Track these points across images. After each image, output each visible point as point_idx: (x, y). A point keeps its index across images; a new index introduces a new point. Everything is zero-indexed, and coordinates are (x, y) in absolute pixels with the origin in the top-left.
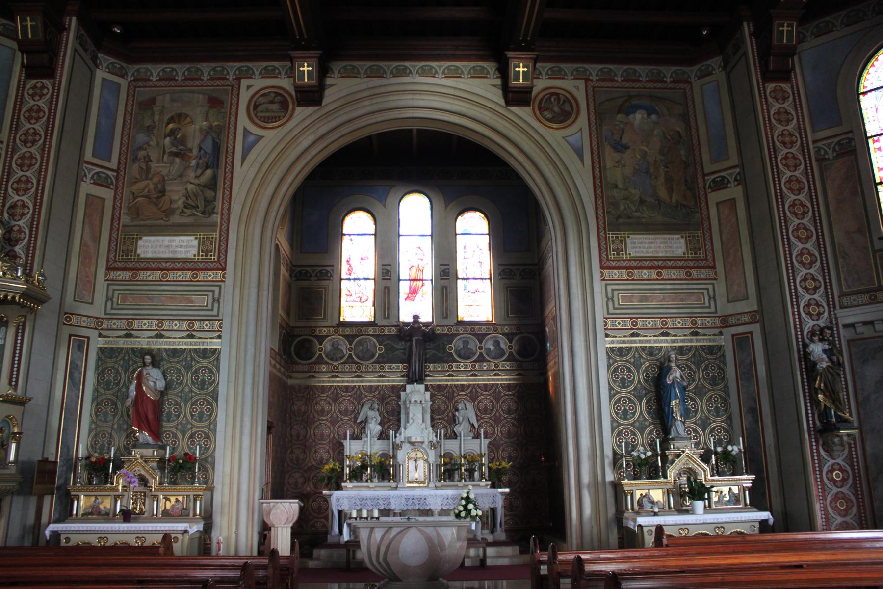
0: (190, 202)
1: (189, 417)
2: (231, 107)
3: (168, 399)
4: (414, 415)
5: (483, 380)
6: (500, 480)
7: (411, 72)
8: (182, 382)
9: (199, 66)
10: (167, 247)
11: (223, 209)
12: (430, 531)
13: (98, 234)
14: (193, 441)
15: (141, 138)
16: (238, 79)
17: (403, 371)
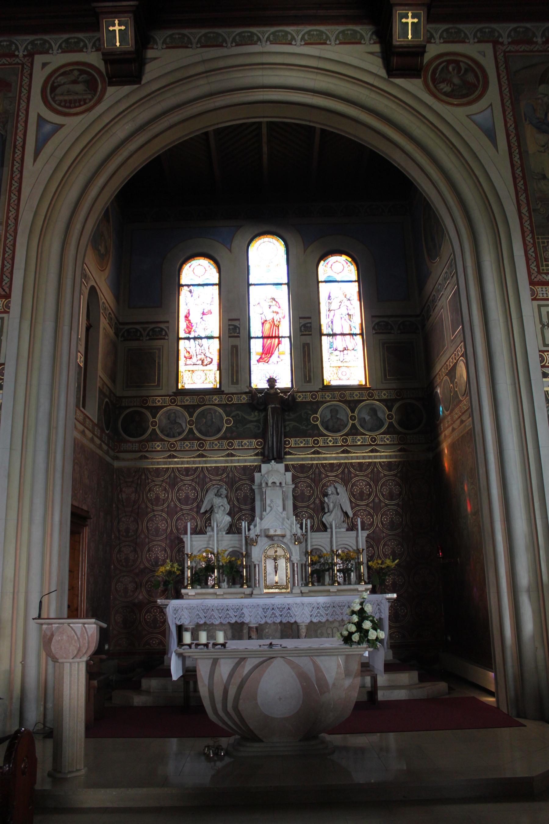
2: (20, 90)
4: (272, 501)
5: (357, 458)
6: (382, 582)
7: (259, 39)
12: (305, 663)
16: (31, 55)
17: (256, 448)
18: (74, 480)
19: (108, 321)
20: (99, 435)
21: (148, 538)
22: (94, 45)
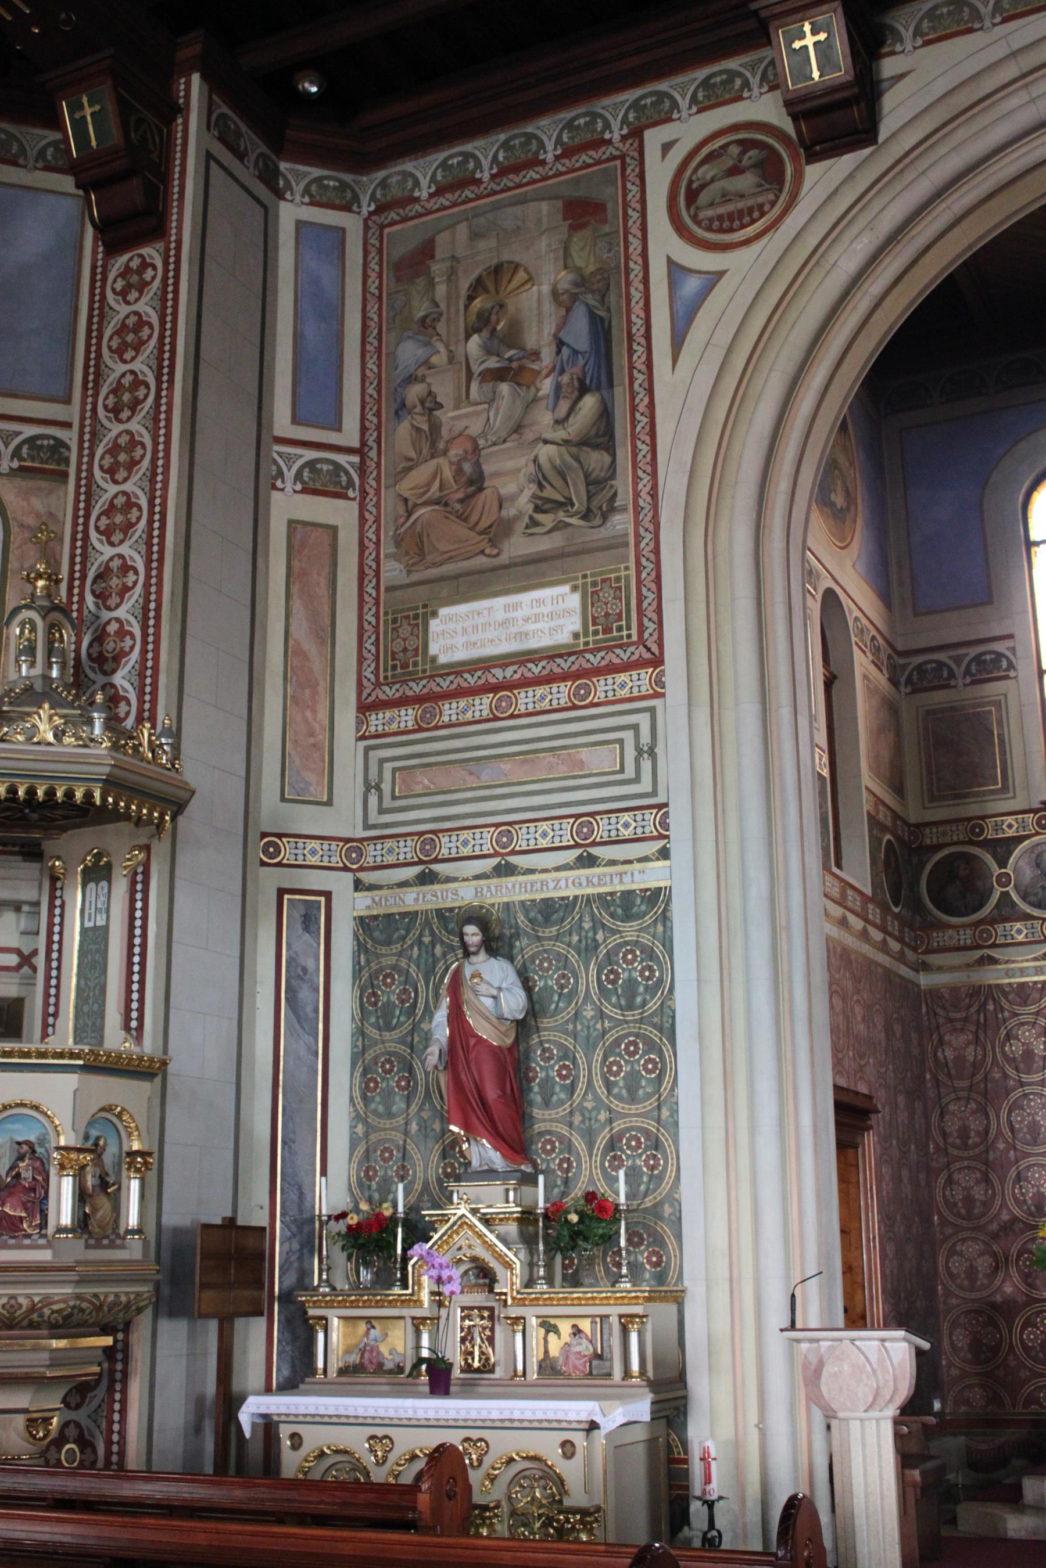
0: (549, 493)
1: (601, 1091)
3: (541, 1043)
8: (574, 992)
9: (530, 129)
10: (503, 623)
11: (637, 495)
13: (327, 621)
14: (614, 1158)
15: (409, 352)
16: (636, 134)
18: (834, 1030)
19: (871, 657)
20: (878, 921)
21: (1015, 1149)
22: (764, 78)
